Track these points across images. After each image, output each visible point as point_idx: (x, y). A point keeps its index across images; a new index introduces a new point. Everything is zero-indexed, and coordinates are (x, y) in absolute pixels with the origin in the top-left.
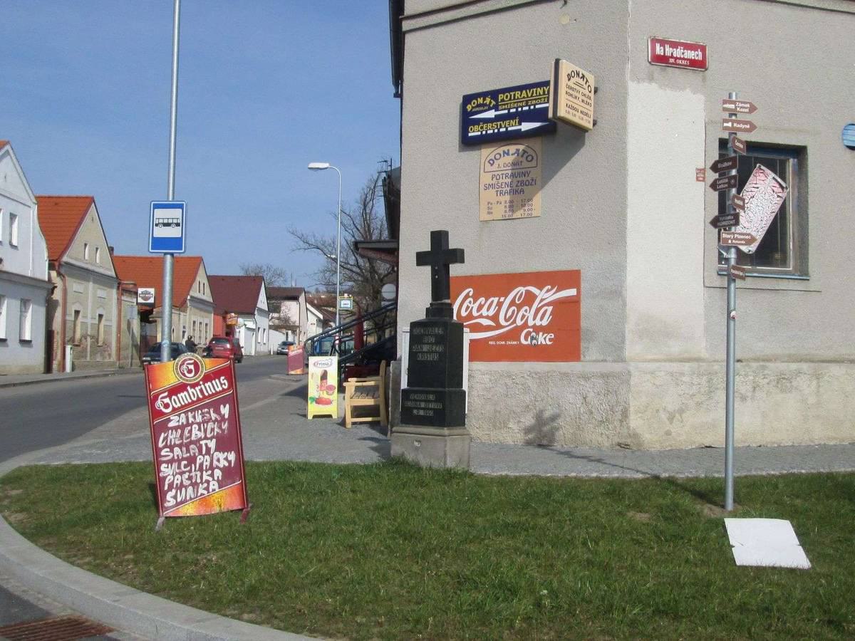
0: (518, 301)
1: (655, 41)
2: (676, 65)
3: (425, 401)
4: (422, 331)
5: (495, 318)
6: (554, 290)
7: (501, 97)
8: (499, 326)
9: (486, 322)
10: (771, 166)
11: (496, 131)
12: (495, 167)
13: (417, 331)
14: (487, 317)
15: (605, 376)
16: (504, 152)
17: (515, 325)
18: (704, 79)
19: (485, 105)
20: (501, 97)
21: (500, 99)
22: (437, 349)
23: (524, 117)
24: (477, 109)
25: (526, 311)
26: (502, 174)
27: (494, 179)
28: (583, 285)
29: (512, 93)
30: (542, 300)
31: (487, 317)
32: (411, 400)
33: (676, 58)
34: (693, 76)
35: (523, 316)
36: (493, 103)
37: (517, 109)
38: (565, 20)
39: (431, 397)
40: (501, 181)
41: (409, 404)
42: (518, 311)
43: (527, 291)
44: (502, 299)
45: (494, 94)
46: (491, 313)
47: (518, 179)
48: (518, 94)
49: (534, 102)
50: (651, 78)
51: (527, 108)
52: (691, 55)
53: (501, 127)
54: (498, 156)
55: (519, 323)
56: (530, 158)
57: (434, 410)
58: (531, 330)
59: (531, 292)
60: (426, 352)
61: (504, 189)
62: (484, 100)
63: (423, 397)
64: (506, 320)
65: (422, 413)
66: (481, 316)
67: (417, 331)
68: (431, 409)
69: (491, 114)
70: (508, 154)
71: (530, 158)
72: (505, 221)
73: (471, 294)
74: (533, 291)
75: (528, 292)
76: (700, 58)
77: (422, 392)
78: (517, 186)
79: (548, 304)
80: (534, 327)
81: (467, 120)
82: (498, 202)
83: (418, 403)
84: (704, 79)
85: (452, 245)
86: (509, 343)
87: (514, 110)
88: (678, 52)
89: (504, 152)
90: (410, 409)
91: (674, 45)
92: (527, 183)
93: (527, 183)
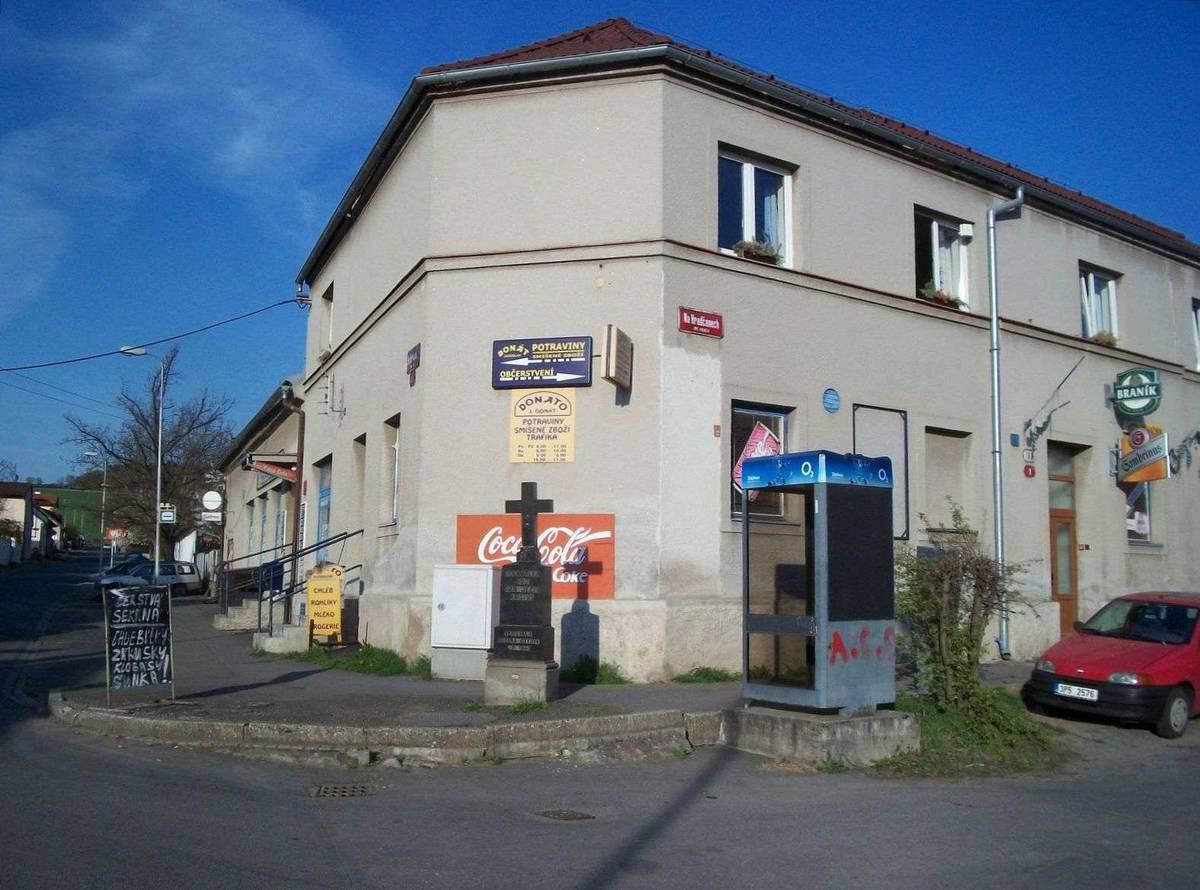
1: (683, 310)
2: (699, 333)
6: (587, 533)
7: (535, 347)
10: (768, 423)
11: (530, 378)
12: (526, 412)
13: (509, 574)
15: (637, 613)
16: (536, 399)
18: (720, 346)
19: (519, 352)
20: (535, 347)
21: (534, 349)
23: (559, 368)
24: (510, 356)
28: (617, 528)
29: (547, 345)
30: (575, 541)
33: (700, 327)
34: (711, 342)
35: (556, 556)
36: (527, 351)
37: (552, 359)
38: (601, 282)
39: (528, 633)
40: (532, 426)
41: (504, 640)
42: (550, 551)
43: (561, 533)
45: (528, 343)
47: (551, 425)
48: (553, 346)
49: (569, 355)
50: (679, 344)
51: (563, 360)
52: (710, 324)
53: (535, 375)
54: (529, 402)
56: (563, 407)
59: (565, 534)
62: (517, 348)
63: (519, 634)
65: (518, 648)
69: (525, 362)
70: (540, 401)
71: (563, 407)
73: (500, 532)
75: (561, 533)
76: (717, 327)
81: (498, 365)
84: (720, 346)
85: (541, 496)
87: (549, 361)
88: (701, 321)
89: (536, 399)
90: (505, 645)
91: (698, 314)
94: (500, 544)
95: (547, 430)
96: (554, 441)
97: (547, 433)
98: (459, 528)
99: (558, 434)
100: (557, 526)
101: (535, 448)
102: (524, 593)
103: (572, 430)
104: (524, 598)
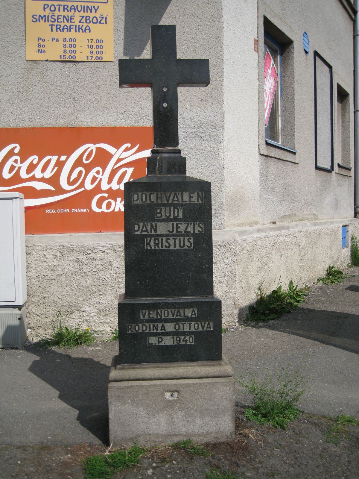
0: (87, 160)
3: (175, 321)
4: (153, 198)
5: (54, 180)
8: (60, 191)
9: (40, 186)
13: (139, 199)
14: (43, 180)
17: (83, 189)
22: (190, 229)
25: (98, 172)
26: (60, 5)
27: (48, 10)
30: (119, 160)
31: (43, 180)
32: (142, 321)
35: (94, 179)
39: (188, 313)
40: (57, 13)
41: (139, 328)
43: (97, 149)
44: (63, 158)
46: (48, 174)
47: (82, 14)
55: (89, 186)
57: (196, 334)
58: (106, 195)
60: (167, 235)
61: (62, 24)
64: (70, 183)
65: (168, 341)
66: (33, 179)
67: (139, 199)
68: (190, 333)
72: (64, 64)
73: (17, 151)
74: (135, 148)
77: (167, 306)
78: (80, 22)
79: (128, 165)
80: (110, 191)
82: (53, 39)
83: (160, 325)
86: (74, 211)
92: (95, 20)
93: (95, 20)
94: (17, 165)
95: (77, 19)
96: (87, 35)
97: (77, 19)
98: (170, 26)
99: (91, 25)
100: (95, 143)
101: (61, 42)
102: (168, 234)
103: (110, 20)
104: (174, 244)
